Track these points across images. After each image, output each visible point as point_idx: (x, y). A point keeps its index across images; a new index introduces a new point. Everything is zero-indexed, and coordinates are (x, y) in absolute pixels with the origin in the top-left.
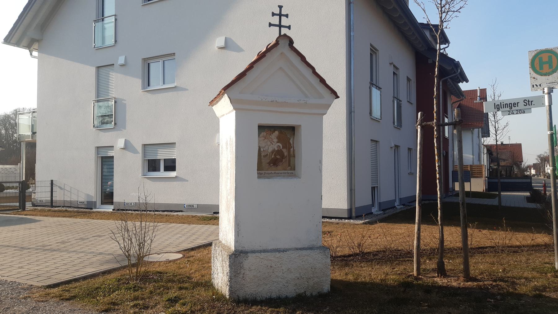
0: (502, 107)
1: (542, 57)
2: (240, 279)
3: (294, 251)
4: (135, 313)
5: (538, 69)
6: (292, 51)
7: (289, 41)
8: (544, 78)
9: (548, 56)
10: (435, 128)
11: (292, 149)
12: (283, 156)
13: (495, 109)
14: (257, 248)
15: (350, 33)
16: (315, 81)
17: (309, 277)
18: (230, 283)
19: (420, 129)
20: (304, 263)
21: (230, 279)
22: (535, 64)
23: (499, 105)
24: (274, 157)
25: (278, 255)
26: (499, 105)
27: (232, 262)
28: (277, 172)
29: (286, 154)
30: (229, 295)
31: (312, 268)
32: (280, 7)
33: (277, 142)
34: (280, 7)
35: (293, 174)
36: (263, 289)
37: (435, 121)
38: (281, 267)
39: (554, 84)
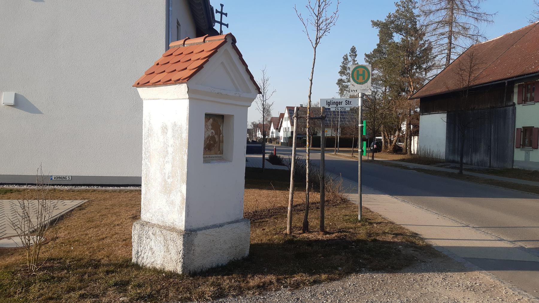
0: (332, 104)
1: (358, 71)
2: (191, 255)
3: (228, 225)
4: (154, 302)
5: (356, 79)
6: (233, 49)
7: (232, 39)
8: (359, 85)
9: (363, 70)
10: (308, 120)
11: (221, 135)
12: (215, 142)
13: (327, 105)
14: (201, 226)
15: (169, 7)
16: (246, 77)
17: (237, 245)
18: (183, 260)
19: (296, 120)
20: (234, 234)
21: (183, 257)
22: (354, 74)
23: (329, 102)
24: (209, 142)
25: (217, 229)
26: (329, 102)
27: (186, 241)
28: (211, 156)
29: (217, 140)
30: (182, 271)
31: (239, 238)
32: (222, 6)
33: (212, 129)
34: (222, 6)
35: (221, 157)
36: (207, 261)
37: (308, 115)
38: (220, 240)
39: (365, 91)
